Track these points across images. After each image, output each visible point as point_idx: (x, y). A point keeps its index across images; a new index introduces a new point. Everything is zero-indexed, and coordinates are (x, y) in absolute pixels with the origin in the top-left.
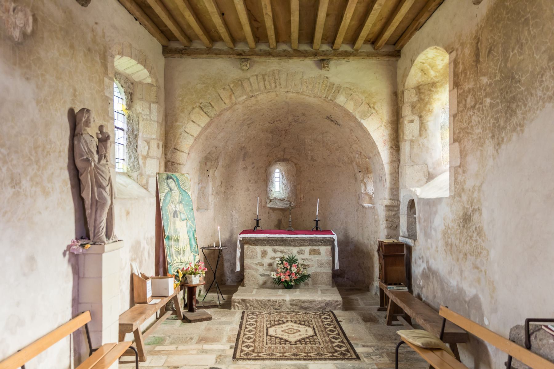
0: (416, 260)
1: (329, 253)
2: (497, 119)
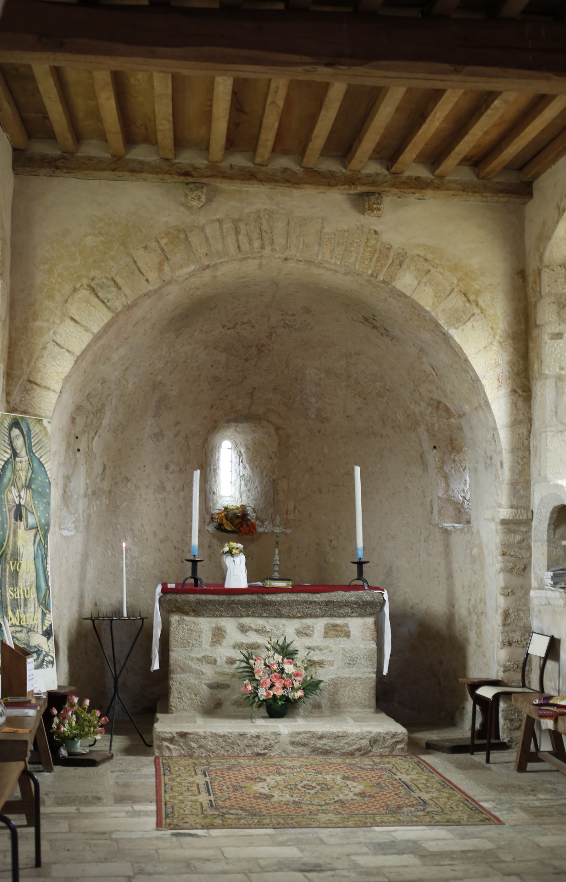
1: (370, 633)
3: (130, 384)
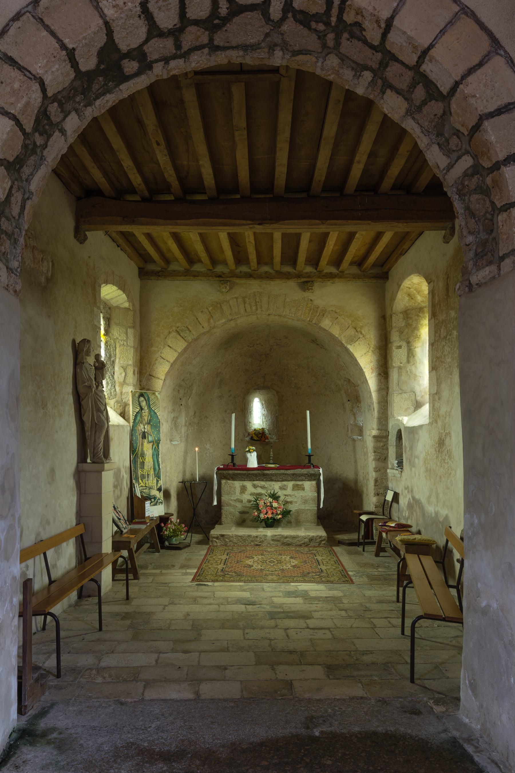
1: (314, 488)
3: (205, 374)
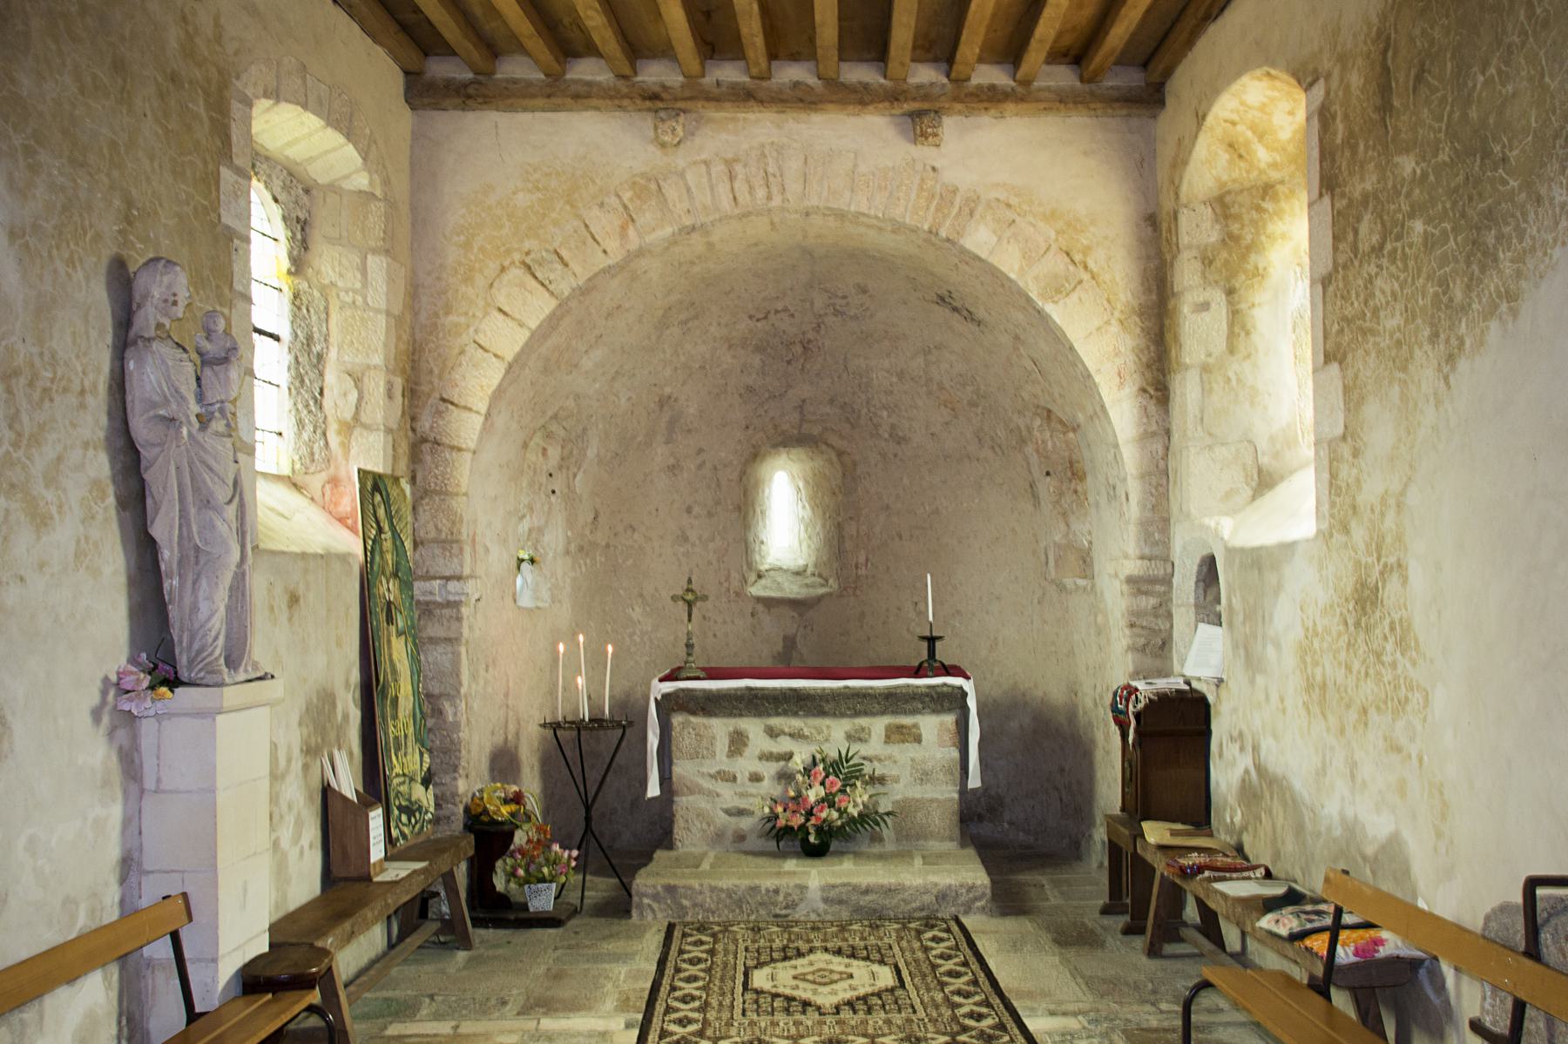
0: (1221, 745)
2: (1444, 283)
